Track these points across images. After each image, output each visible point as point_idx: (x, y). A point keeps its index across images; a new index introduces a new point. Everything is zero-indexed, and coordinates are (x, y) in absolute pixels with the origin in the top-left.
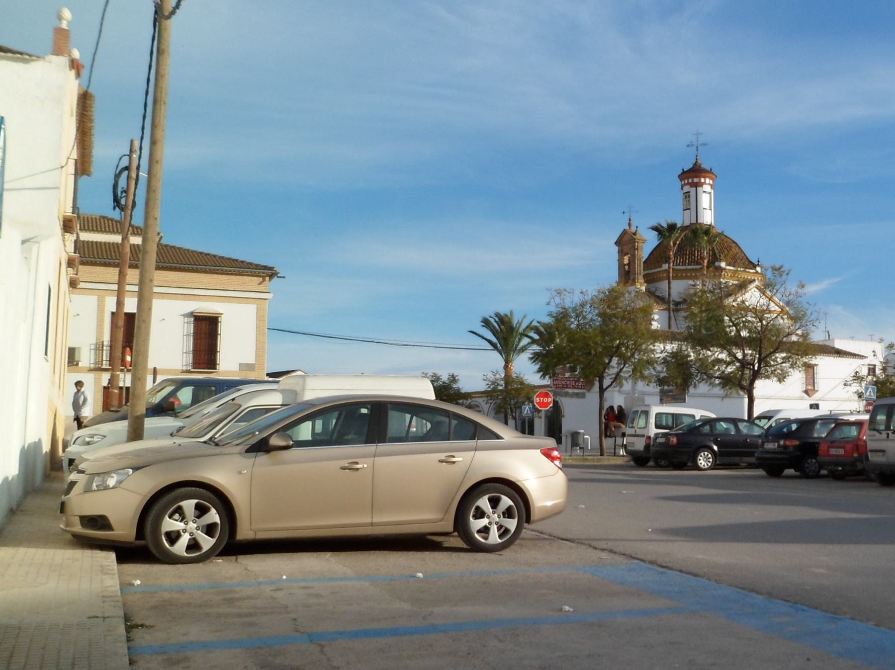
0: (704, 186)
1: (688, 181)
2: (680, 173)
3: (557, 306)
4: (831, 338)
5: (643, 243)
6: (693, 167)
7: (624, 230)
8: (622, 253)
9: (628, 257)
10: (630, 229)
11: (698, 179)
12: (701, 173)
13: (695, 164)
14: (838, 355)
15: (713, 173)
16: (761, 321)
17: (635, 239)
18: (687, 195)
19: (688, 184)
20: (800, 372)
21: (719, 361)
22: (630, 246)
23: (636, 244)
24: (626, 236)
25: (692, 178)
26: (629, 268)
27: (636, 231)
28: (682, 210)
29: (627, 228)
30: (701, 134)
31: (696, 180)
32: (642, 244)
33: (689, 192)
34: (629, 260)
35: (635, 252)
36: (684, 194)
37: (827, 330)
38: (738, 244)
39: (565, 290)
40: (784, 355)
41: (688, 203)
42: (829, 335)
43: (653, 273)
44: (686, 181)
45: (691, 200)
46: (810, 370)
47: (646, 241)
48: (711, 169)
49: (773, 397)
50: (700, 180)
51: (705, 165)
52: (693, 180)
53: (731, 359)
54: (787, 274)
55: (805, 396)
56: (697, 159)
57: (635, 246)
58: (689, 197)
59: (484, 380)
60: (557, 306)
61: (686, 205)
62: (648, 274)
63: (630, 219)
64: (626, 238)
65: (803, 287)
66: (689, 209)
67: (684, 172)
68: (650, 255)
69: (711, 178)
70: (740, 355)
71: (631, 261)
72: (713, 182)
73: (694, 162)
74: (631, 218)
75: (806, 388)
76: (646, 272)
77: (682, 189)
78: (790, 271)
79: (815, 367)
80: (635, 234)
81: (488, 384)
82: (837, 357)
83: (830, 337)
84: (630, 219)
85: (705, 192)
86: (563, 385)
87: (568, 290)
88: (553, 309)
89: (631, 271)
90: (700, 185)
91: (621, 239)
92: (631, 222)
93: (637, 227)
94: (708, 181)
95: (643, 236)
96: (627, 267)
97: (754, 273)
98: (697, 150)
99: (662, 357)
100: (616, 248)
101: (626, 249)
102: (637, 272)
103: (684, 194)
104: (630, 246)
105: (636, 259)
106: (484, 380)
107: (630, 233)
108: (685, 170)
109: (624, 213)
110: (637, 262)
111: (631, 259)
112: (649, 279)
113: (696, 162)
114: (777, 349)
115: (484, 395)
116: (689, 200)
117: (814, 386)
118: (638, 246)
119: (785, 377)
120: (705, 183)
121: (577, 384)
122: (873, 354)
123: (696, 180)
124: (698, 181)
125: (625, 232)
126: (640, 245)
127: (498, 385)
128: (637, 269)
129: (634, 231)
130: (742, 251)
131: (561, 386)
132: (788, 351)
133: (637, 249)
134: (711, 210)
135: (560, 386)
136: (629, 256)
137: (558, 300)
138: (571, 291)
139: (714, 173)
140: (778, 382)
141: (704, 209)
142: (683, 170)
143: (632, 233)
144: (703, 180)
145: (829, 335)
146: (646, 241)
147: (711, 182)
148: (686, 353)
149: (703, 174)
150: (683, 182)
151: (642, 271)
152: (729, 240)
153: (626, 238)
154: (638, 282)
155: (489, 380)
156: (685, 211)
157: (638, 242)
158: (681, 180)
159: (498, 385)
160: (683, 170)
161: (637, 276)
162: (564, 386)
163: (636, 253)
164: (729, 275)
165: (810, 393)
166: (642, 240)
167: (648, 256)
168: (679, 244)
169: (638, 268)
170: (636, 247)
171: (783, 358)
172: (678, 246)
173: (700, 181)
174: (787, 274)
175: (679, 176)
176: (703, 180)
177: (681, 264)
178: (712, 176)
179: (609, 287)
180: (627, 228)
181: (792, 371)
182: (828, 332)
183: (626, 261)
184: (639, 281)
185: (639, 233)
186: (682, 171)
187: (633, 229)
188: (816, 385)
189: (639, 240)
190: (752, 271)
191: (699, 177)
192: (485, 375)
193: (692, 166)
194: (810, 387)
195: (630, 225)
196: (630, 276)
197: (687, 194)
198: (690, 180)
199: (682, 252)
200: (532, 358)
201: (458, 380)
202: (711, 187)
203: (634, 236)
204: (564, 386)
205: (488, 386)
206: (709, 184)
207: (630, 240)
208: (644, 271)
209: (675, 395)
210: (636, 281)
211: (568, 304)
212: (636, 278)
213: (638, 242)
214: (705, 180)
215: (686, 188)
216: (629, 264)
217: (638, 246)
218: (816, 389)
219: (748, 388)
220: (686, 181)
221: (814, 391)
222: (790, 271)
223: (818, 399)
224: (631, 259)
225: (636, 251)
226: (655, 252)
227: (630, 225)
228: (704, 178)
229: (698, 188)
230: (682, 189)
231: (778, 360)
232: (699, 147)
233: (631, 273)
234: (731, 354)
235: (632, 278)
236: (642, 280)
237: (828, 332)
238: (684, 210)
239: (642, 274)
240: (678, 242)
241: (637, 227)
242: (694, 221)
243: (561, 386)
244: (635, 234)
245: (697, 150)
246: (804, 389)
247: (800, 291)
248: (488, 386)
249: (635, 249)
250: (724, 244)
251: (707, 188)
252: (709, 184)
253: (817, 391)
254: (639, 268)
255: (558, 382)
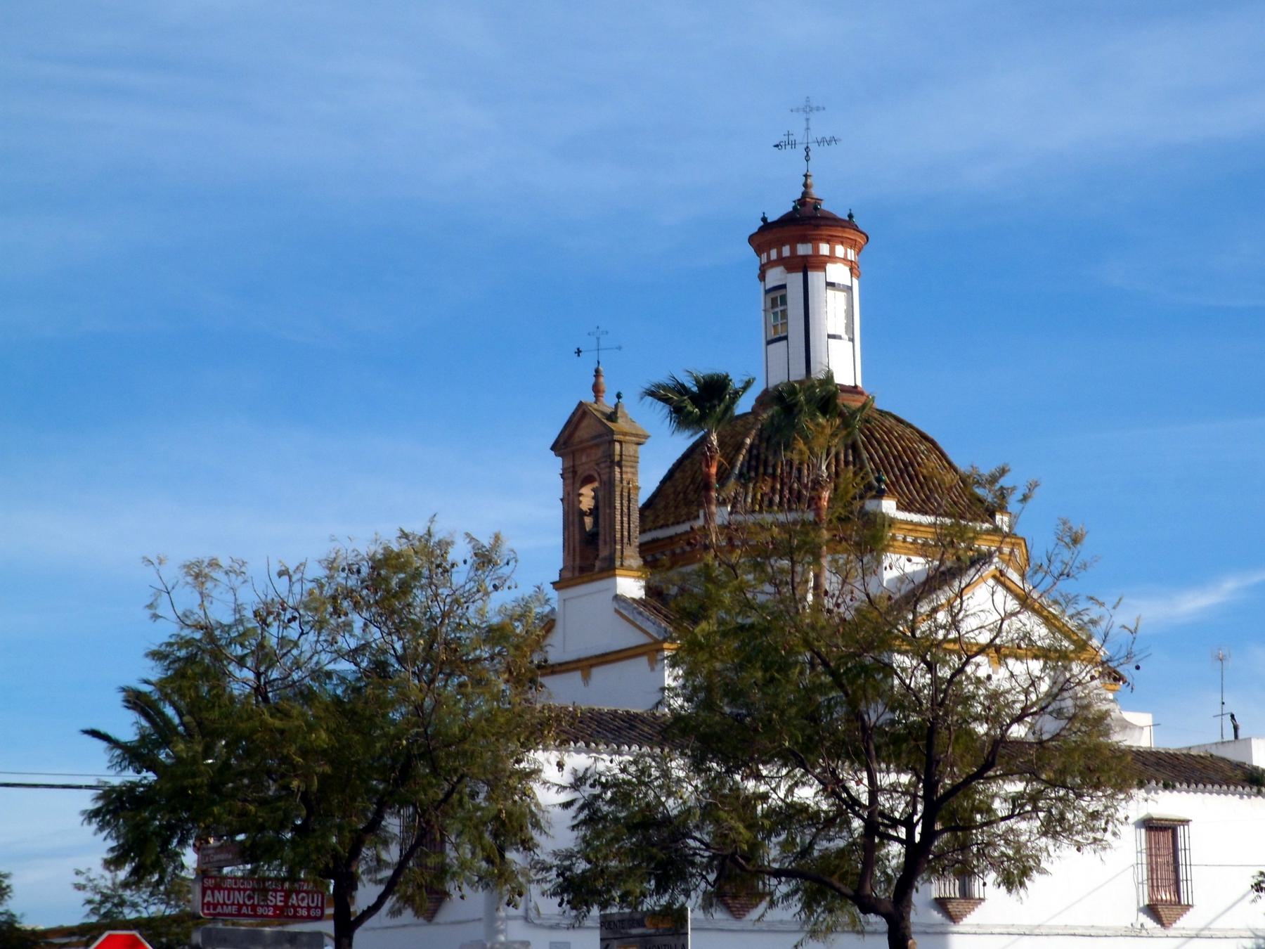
0: (829, 267)
1: (779, 253)
2: (755, 230)
3: (182, 620)
4: (1241, 736)
5: (639, 444)
6: (795, 208)
7: (581, 404)
8: (573, 478)
9: (593, 490)
10: (596, 403)
11: (810, 246)
12: (817, 227)
13: (802, 202)
14: (1255, 789)
15: (856, 229)
16: (931, 668)
17: (612, 432)
18: (777, 296)
19: (781, 261)
20: (1079, 850)
21: (794, 814)
22: (599, 453)
23: (617, 446)
24: (585, 423)
25: (793, 242)
26: (596, 523)
27: (616, 406)
28: (764, 342)
29: (589, 398)
30: (818, 109)
31: (803, 249)
32: (635, 447)
33: (784, 287)
34: (595, 498)
35: (612, 473)
36: (767, 292)
37: (1227, 709)
38: (941, 445)
39: (214, 564)
40: (1015, 787)
41: (780, 322)
42: (1236, 728)
43: (671, 538)
44: (774, 254)
45: (790, 312)
46: (1165, 838)
47: (647, 437)
48: (850, 216)
49: (1044, 931)
50: (816, 249)
51: (833, 205)
52: (793, 250)
53: (833, 805)
54: (1025, 498)
55: (1150, 923)
56: (806, 185)
57: (612, 455)
58: (784, 300)
59: (79, 887)
60: (182, 620)
61: (775, 327)
62: (654, 541)
63: (597, 373)
64: (585, 431)
65: (1076, 540)
66: (786, 338)
67: (767, 226)
68: (663, 482)
69: (852, 244)
70: (861, 792)
71: (601, 504)
72: (858, 253)
73: (799, 196)
74: (601, 368)
75: (1151, 899)
76: (648, 537)
77: (762, 277)
78: (1033, 486)
79: (1180, 830)
80: (612, 417)
81: (89, 902)
82: (1249, 796)
83: (1240, 732)
84: (597, 373)
85: (830, 285)
86: (240, 906)
87: (225, 562)
88: (165, 631)
89: (602, 531)
90: (819, 263)
91: (571, 436)
92: (602, 380)
93: (619, 396)
94: (840, 250)
95: (638, 424)
96: (588, 521)
97: (988, 532)
98: (807, 158)
99: (581, 802)
100: (557, 464)
101: (586, 463)
102: (618, 536)
103: (767, 292)
104: (599, 453)
105: (618, 493)
106: (79, 887)
107: (599, 415)
108: (769, 220)
109: (579, 352)
110: (618, 505)
111: (601, 494)
112: (652, 556)
113: (805, 194)
114: (989, 765)
115: (75, 939)
116: (784, 313)
117: (1178, 892)
118: (621, 455)
119: (1025, 872)
120: (832, 258)
121: (294, 900)
122: (149, 612)
123: (803, 249)
124: (810, 252)
125: (581, 412)
126: (629, 449)
127: (122, 903)
128: (618, 527)
129: (609, 410)
130: (950, 463)
131: (234, 909)
132: (1029, 772)
133: (620, 464)
134: (852, 340)
135: (227, 910)
136: (596, 484)
137: (187, 599)
138: (236, 567)
139: (861, 228)
140: (1003, 889)
141: (830, 336)
142: (764, 219)
143: (603, 413)
144: (824, 249)
145: (1236, 728)
146: (647, 437)
147: (851, 255)
148: (126, 756)
149: (825, 232)
150: (764, 256)
151: (635, 531)
152: (908, 431)
153: (585, 431)
154: (622, 565)
155: (95, 889)
156: (771, 347)
157: (621, 442)
158: (759, 250)
159: (122, 903)
160: (764, 219)
161: (618, 547)
162: (244, 910)
163: (618, 475)
164: (909, 539)
165: (1163, 912)
166: (636, 435)
167: (657, 484)
168: (752, 445)
169: (622, 522)
170: (617, 458)
171: (1015, 800)
172: (750, 451)
173: (816, 254)
174: (1025, 498)
175: (751, 239)
176: (824, 249)
177: (757, 507)
178: (850, 234)
179: (373, 548)
180: (589, 398)
181: (1051, 848)
182: (1232, 716)
183: (587, 502)
184: (626, 563)
185: (625, 416)
186: (762, 223)
187: (608, 403)
188: (1183, 886)
189: (625, 434)
190: (986, 526)
191: (815, 240)
192: (83, 870)
193: (791, 209)
194: (1165, 896)
195: (597, 389)
196: (597, 550)
197: (778, 294)
198: (786, 251)
199: (761, 470)
200: (95, 814)
201: (8, 887)
202: (851, 270)
203: (609, 424)
204: (244, 910)
205: (89, 907)
206: (844, 260)
207: (600, 436)
208: (642, 532)
209: (650, 935)
210: (618, 563)
211: (221, 613)
212: (618, 554)
213: (621, 442)
214: (832, 250)
215: (776, 276)
216: (594, 512)
217: (621, 455)
218: (1184, 901)
219: (890, 908)
220: (774, 254)
221: (1180, 906)
222: (1033, 486)
223: (1193, 933)
224: (601, 494)
225: (617, 470)
226: (678, 475)
227: (597, 389)
228: (828, 242)
229: (810, 274)
230: (762, 277)
231: (997, 804)
232: (813, 147)
233: (601, 537)
234: (832, 786)
235: (604, 552)
236: (634, 561)
237: (1232, 716)
238: (769, 343)
239: (636, 542)
240: (748, 441)
241: (619, 396)
242: (798, 373)
243: (234, 909)
244: (612, 417)
245: (807, 158)
246: (1147, 902)
247: (1066, 555)
248: (89, 907)
249: (612, 462)
250: (891, 444)
251: (837, 272)
252: (844, 260)
253: (1189, 906)
254: (627, 524)
255: (220, 896)
